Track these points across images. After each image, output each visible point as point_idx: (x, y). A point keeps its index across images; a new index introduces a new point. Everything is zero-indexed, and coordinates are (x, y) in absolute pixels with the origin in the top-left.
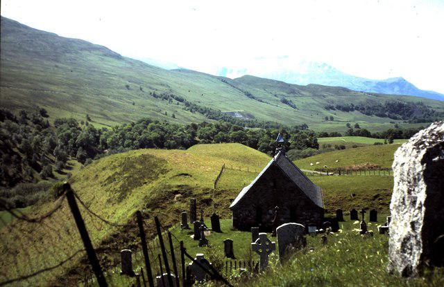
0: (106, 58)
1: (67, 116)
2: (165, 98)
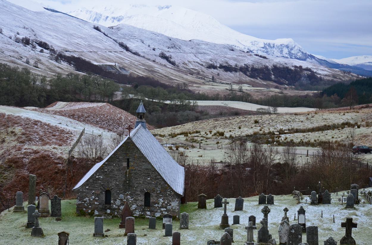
2: (26, 42)
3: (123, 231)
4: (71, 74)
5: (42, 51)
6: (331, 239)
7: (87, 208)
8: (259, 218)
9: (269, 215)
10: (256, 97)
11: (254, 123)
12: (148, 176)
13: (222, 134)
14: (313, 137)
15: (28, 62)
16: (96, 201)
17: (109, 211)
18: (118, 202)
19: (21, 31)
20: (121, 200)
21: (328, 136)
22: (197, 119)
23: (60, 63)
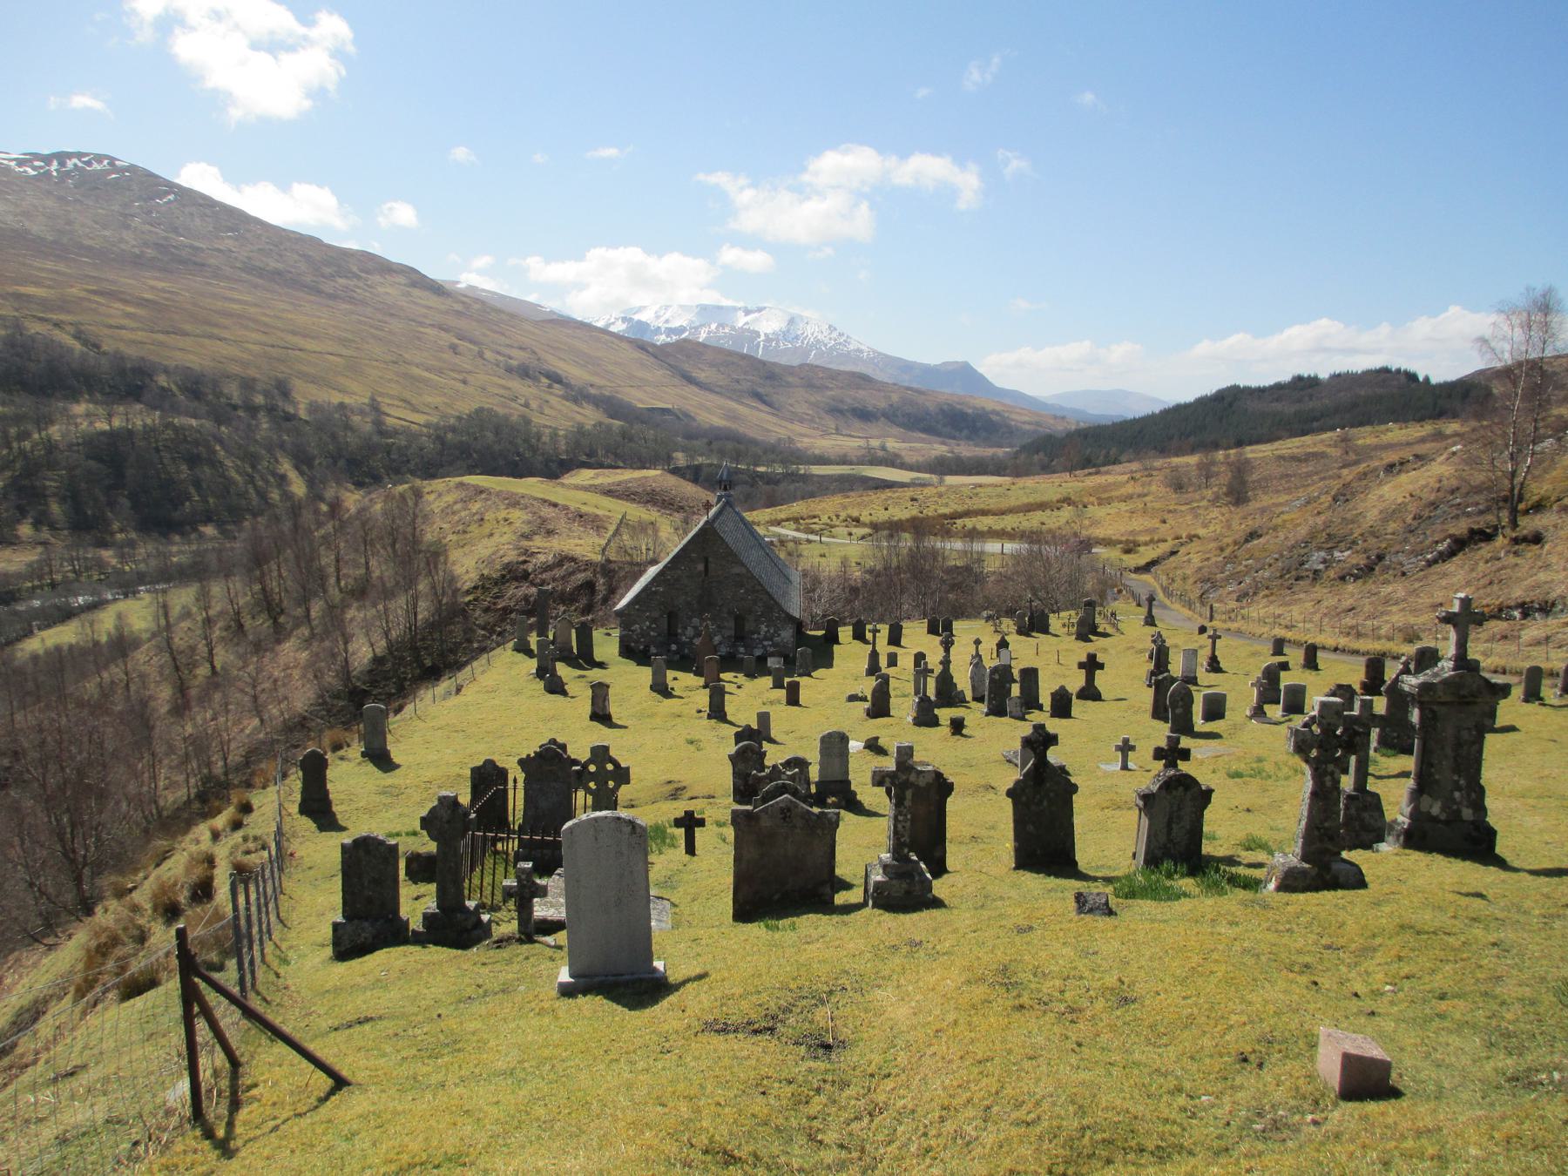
0: (416, 292)
1: (1365, 526)
2: (524, 373)
3: (701, 681)
4: (600, 424)
5: (550, 386)
6: (1063, 688)
7: (637, 642)
8: (934, 659)
9: (953, 650)
10: (910, 458)
12: (742, 586)
13: (857, 520)
14: (1009, 522)
15: (526, 405)
17: (674, 647)
18: (690, 632)
19: (515, 353)
20: (695, 628)
21: (1032, 521)
22: (812, 495)
23: (581, 406)
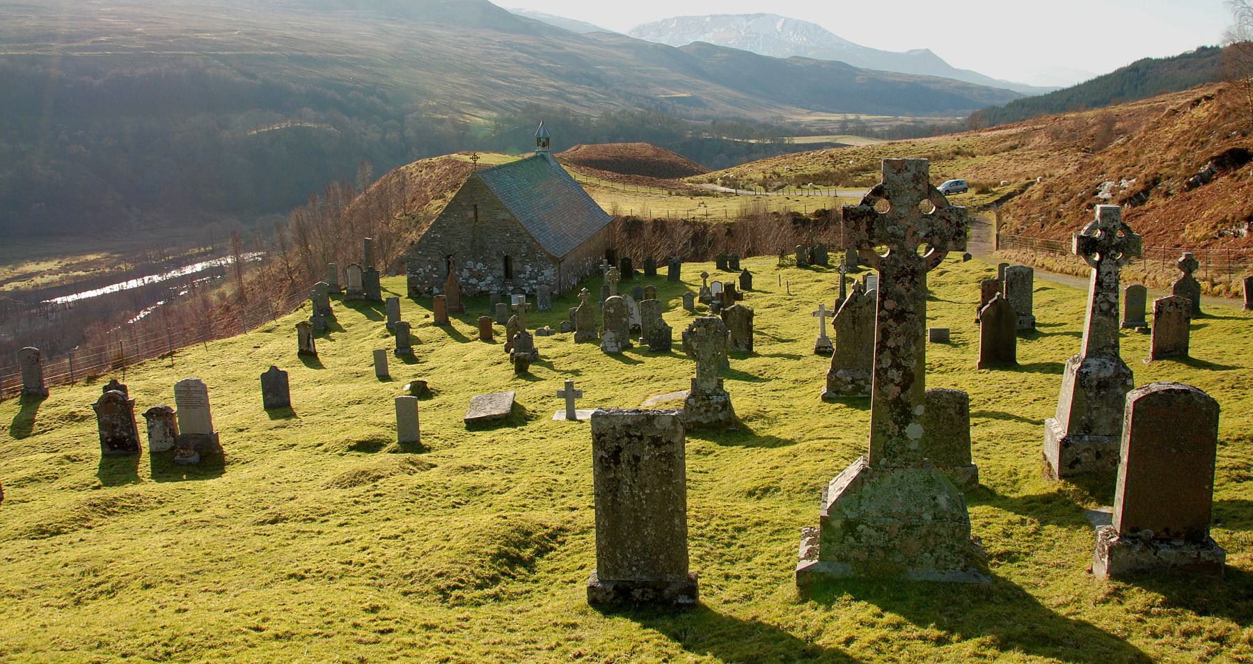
6: (274, 368)
7: (422, 283)
11: (934, 169)
16: (435, 272)
18: (466, 273)
20: (470, 270)
